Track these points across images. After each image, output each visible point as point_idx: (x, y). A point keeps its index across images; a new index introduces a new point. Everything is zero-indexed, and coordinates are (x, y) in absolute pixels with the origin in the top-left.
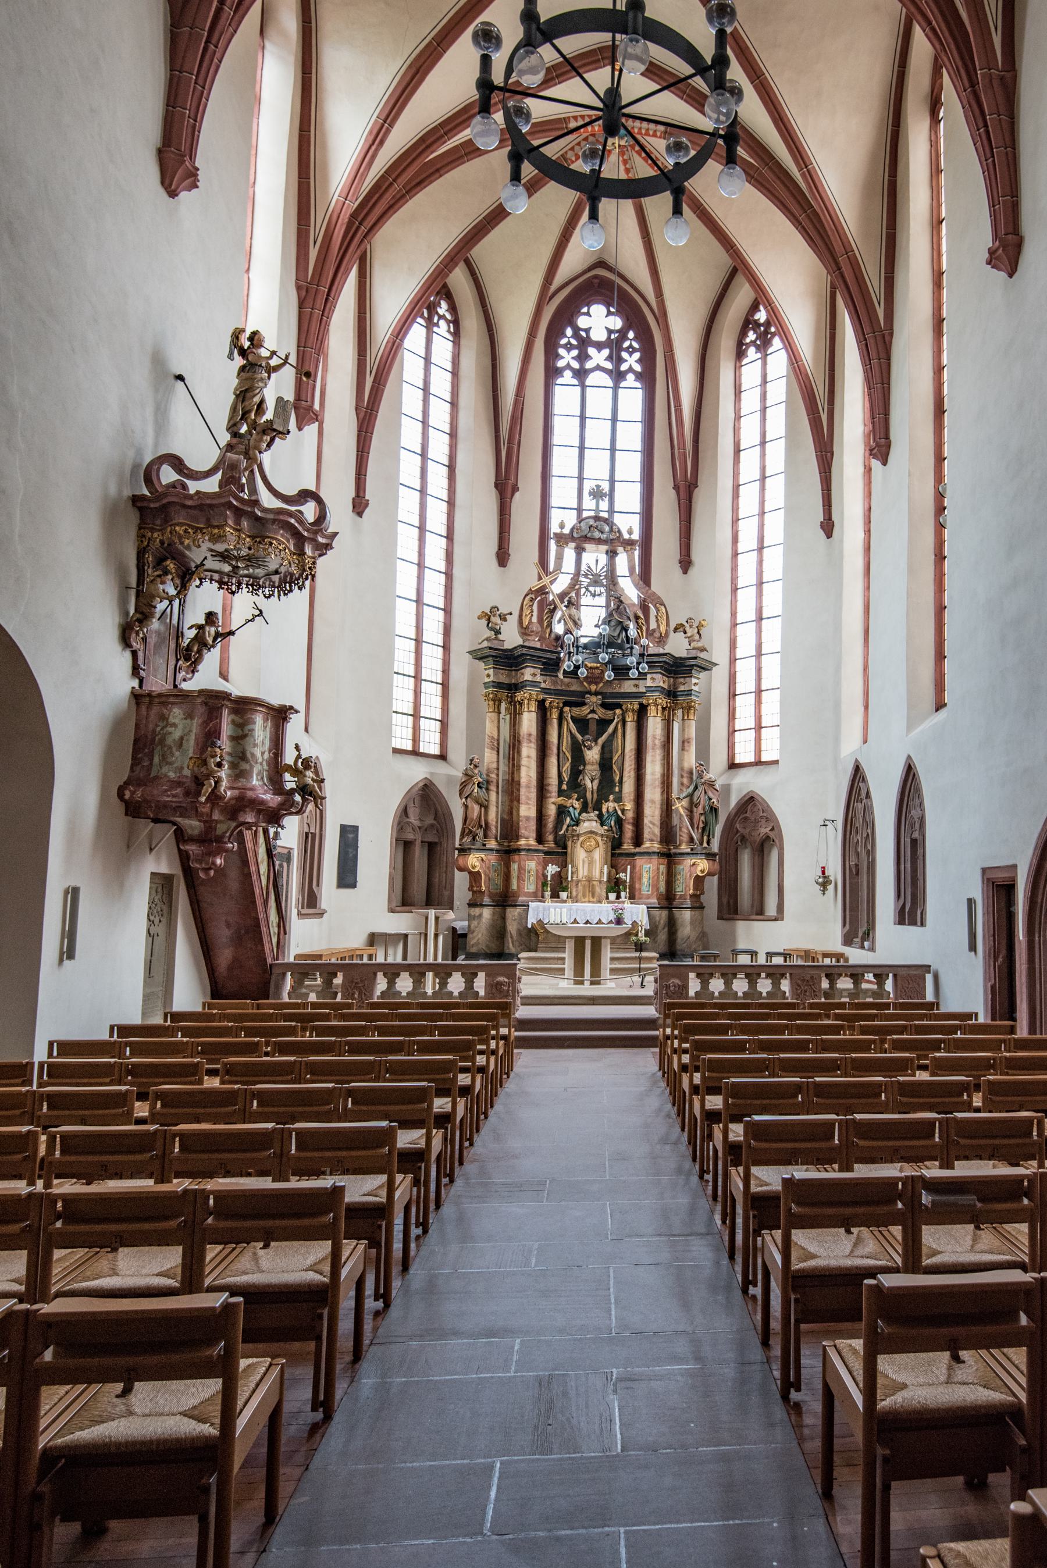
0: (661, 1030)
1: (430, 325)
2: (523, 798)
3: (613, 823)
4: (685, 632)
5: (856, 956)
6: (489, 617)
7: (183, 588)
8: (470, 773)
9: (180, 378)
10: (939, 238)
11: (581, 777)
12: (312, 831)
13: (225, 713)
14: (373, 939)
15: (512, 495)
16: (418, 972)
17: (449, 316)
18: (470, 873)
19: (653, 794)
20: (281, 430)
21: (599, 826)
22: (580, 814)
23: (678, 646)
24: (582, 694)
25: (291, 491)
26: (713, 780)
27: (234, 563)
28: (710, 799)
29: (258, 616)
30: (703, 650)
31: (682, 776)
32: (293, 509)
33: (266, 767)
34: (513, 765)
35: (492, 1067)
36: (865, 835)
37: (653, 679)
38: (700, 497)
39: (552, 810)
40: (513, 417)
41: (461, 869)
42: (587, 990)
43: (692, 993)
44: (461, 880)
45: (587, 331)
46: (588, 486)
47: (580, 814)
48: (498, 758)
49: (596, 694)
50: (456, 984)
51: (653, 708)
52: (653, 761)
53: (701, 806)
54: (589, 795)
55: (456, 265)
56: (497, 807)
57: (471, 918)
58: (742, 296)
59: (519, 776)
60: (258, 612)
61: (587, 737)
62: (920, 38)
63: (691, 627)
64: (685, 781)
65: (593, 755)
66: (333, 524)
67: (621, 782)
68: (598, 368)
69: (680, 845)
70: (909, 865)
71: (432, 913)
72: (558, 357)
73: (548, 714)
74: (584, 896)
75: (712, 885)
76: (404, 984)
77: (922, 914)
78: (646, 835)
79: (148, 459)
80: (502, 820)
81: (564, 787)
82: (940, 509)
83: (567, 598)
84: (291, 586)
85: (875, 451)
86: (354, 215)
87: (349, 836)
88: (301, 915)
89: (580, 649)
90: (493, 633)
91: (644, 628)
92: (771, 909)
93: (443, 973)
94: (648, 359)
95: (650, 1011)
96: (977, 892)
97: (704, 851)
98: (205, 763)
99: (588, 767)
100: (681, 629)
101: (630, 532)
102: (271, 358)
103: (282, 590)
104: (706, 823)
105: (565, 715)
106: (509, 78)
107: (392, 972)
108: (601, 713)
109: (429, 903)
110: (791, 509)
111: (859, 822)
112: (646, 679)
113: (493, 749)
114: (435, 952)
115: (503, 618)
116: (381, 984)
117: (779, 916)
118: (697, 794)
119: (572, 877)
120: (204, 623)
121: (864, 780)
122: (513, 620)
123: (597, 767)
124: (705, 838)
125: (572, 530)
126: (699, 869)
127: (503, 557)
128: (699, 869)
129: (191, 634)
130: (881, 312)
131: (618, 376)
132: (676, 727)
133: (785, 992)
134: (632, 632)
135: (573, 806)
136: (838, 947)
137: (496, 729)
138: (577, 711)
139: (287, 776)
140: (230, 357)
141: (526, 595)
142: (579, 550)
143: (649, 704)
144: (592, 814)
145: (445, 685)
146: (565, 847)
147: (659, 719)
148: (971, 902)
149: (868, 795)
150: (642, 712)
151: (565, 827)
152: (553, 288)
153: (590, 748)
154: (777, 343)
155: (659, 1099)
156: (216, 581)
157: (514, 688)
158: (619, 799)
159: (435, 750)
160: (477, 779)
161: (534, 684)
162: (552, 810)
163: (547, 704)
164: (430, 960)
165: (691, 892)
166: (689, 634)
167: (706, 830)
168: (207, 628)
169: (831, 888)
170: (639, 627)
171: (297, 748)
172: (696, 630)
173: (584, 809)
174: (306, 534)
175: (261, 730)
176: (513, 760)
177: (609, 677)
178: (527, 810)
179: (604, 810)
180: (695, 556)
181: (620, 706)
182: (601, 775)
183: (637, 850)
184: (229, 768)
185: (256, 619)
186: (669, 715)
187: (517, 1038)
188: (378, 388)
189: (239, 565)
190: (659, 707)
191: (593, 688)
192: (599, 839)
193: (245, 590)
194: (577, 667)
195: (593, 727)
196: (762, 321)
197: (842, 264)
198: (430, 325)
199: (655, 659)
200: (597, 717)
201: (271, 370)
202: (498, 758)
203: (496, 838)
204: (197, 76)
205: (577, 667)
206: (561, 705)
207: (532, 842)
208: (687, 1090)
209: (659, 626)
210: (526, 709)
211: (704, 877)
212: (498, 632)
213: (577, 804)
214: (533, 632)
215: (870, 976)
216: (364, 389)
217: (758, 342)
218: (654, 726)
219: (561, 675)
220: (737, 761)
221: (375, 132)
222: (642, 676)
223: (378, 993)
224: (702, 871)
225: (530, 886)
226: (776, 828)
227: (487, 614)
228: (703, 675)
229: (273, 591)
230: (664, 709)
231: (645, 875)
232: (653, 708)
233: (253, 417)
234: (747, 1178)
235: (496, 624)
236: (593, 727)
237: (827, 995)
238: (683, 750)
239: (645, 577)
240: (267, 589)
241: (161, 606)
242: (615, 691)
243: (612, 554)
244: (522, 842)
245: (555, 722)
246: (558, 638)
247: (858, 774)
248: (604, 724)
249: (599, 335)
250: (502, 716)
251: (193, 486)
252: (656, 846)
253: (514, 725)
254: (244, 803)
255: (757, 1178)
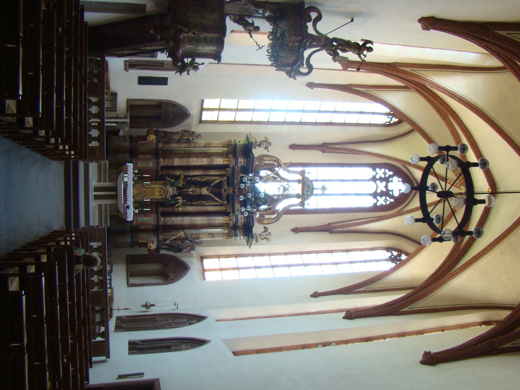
0: (74, 231)
1: (388, 114)
2: (183, 159)
3: (172, 202)
4: (264, 232)
5: (112, 323)
6: (266, 142)
7: (268, 19)
8: (194, 135)
9: (352, 21)
10: (436, 331)
11: (193, 186)
12: (165, 66)
13: (217, 35)
14: (115, 95)
15: (321, 151)
16: (100, 115)
17: (392, 122)
18: (146, 136)
19: (187, 220)
20: (336, 59)
21: (171, 195)
22: (176, 186)
23: (257, 229)
24: (233, 185)
25: (312, 61)
26: (195, 249)
27: (281, 38)
28: (185, 248)
29: (259, 47)
30: (257, 241)
31: (196, 234)
32: (305, 62)
33: (193, 51)
34: (198, 154)
35: (48, 146)
36: (171, 324)
37: (242, 218)
38: (326, 235)
39: (178, 173)
40: (354, 150)
41: (148, 131)
42: (92, 193)
43: (92, 244)
44: (143, 131)
45: (392, 181)
46: (326, 184)
47: (176, 186)
48: (201, 147)
49: (234, 192)
50: (95, 133)
51: (228, 219)
52: (203, 220)
53: (181, 244)
54: (185, 190)
55: (411, 126)
56: (178, 148)
57: (124, 137)
58: (410, 247)
59: (192, 158)
60: (261, 47)
61: (213, 188)
62: (506, 314)
63: (267, 234)
64: (194, 236)
65: (205, 191)
66: (299, 78)
67: (192, 205)
68: (377, 186)
69: (163, 235)
70: (158, 345)
71: (128, 120)
72: (380, 168)
73: (223, 170)
74: (136, 190)
75: (144, 251)
76: (94, 110)
77: (134, 353)
78: (167, 219)
79: (319, 8)
80: (172, 150)
81: (189, 178)
82: (325, 345)
83: (276, 176)
84: (272, 60)
85: (349, 313)
86: (424, 86)
87: (163, 81)
88: (126, 62)
89: (253, 185)
90: (259, 144)
91: (265, 213)
92: (132, 281)
93: (100, 127)
94: (383, 208)
95: (82, 224)
96: (148, 377)
97: (160, 247)
98: (195, 27)
99: (198, 189)
100: (265, 230)
101: (308, 204)
102: (364, 55)
103: (271, 57)
104: (174, 247)
105: (223, 178)
106: (450, 157)
107: (100, 104)
108: (225, 194)
109: (131, 117)
110: (322, 278)
111: (177, 321)
112: (241, 215)
113: (206, 144)
114: (110, 123)
115: (266, 148)
116: (94, 100)
117: (129, 285)
118: (188, 242)
119: (145, 184)
120: (255, 26)
121: (198, 321)
122: (265, 152)
123: (199, 193)
124: (166, 247)
125: (307, 178)
126: (151, 245)
127: (294, 147)
128: (151, 245)
129: (250, 21)
130: (406, 309)
131: (375, 195)
132: (219, 230)
133: (94, 289)
134: (263, 207)
135: (179, 183)
136: (116, 314)
137: (215, 146)
138: (225, 183)
139: (190, 60)
140: (362, 40)
141: (277, 158)
142: (299, 181)
143: (229, 217)
144: (176, 192)
145: (234, 122)
146: (160, 180)
147: (223, 222)
148: (142, 374)
149: (191, 324)
150: (225, 214)
151: (169, 179)
152: (407, 166)
153: (207, 190)
154: (393, 265)
155: (43, 231)
156: (272, 31)
157: (235, 157)
158: (184, 204)
159: (204, 118)
160: (191, 138)
161: (237, 163)
162: (178, 173)
163: (228, 169)
164: (106, 120)
165: (140, 241)
166: (263, 234)
167: (170, 247)
168: (252, 27)
169: (145, 309)
170: (265, 210)
171: (203, 64)
172: (265, 237)
173: (178, 188)
174: (294, 67)
175: (210, 49)
176: (201, 154)
177: (241, 198)
178: (177, 162)
179: (178, 198)
180: (300, 235)
181: (228, 203)
182: (195, 196)
183: (159, 214)
184: (193, 37)
185: (258, 46)
186: (225, 227)
187: (69, 163)
188: (359, 93)
189: (280, 41)
190: (228, 222)
191: (236, 190)
192: (164, 196)
193: (270, 42)
194: (244, 183)
195: (218, 191)
196: (401, 258)
197: (424, 290)
198: (388, 114)
199: (251, 219)
200: (222, 192)
201: (359, 55)
202: (201, 147)
203: (163, 147)
204: (461, 32)
205: (244, 183)
206: (227, 175)
207: (162, 164)
208: (48, 244)
209: (266, 219)
210: (225, 160)
211: (147, 247)
212: (259, 146)
213: (180, 185)
214: (261, 161)
215: (103, 329)
216: (359, 88)
217: (393, 257)
218: (219, 220)
219: (241, 175)
220: (205, 260)
221: (454, 94)
222: (242, 213)
223: (90, 98)
224: (150, 246)
225: (140, 164)
226: (173, 281)
227: (267, 140)
228: (245, 242)
229: (270, 53)
230: (228, 224)
231: (147, 219)
232: (228, 219)
233: (339, 47)
234: (14, 275)
235: (263, 145)
236: (218, 191)
237: (93, 309)
238: (209, 234)
239: (288, 211)
240: (271, 51)
241: (261, 11)
242: (235, 200)
243: (298, 196)
244: (162, 160)
245: (219, 173)
246: (258, 173)
247: (200, 318)
248: (220, 196)
249: (390, 186)
250: (221, 148)
251: (310, 25)
252: (161, 223)
253: (217, 154)
254: (178, 43)
255: (14, 279)
